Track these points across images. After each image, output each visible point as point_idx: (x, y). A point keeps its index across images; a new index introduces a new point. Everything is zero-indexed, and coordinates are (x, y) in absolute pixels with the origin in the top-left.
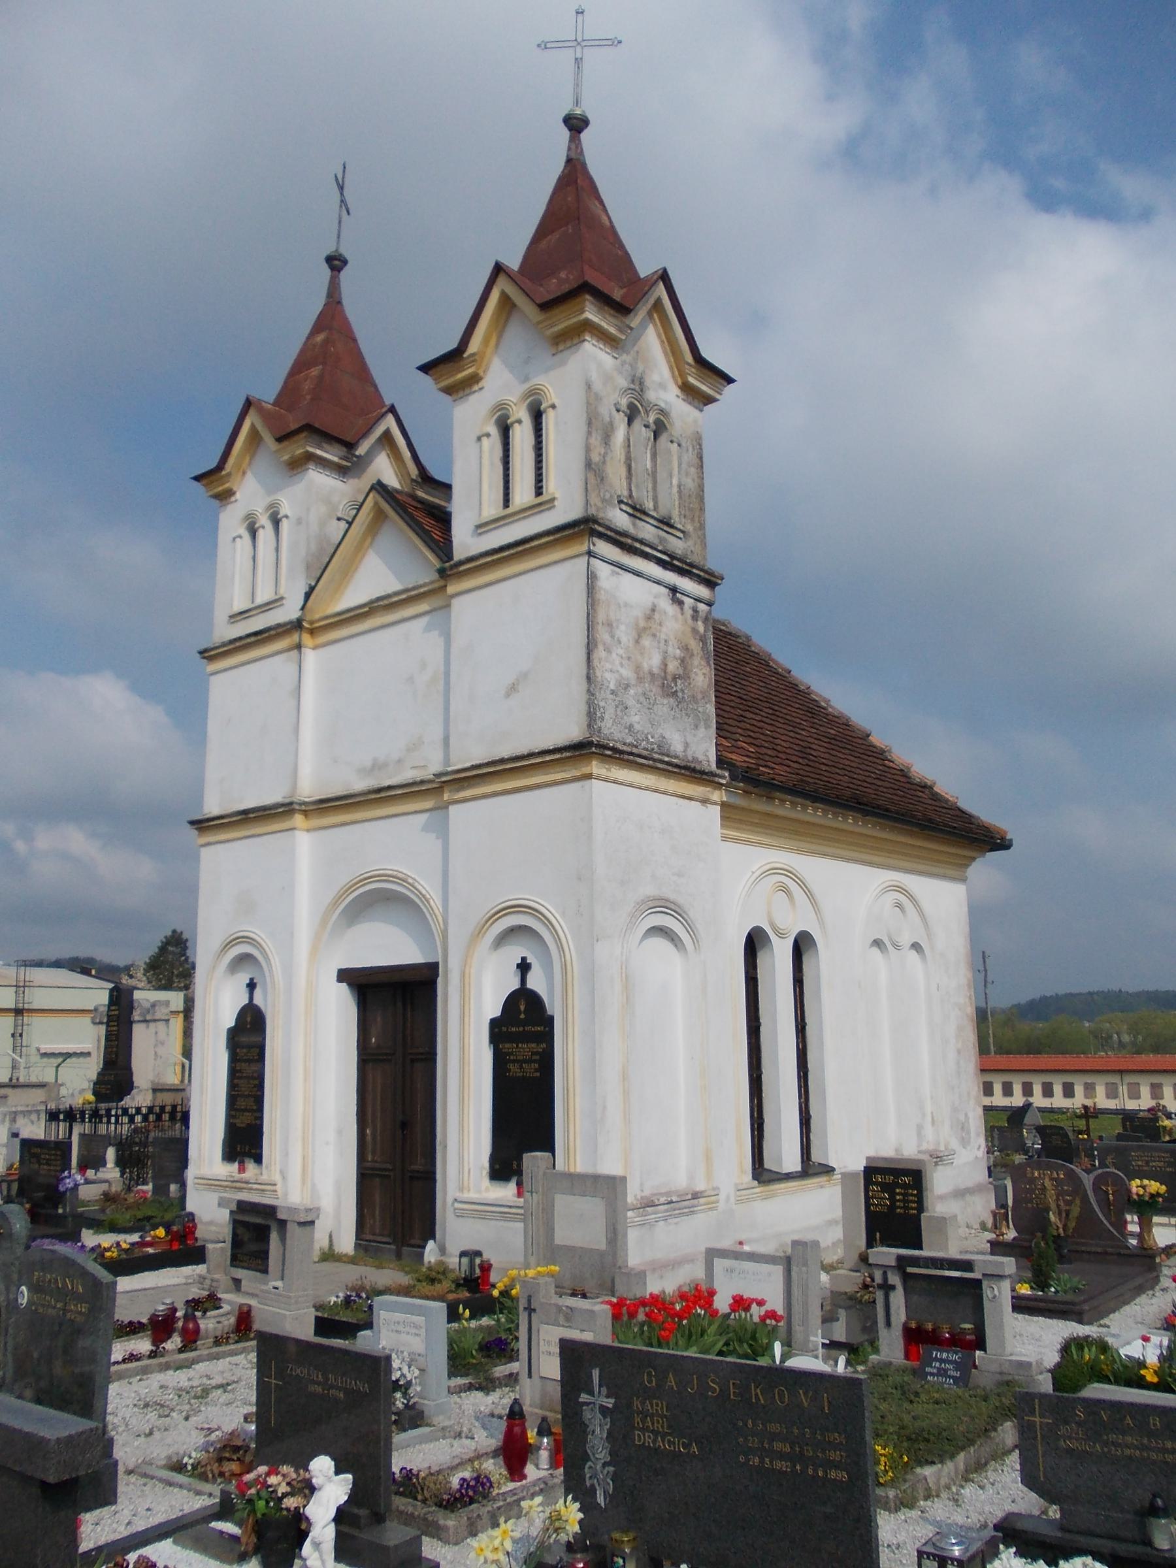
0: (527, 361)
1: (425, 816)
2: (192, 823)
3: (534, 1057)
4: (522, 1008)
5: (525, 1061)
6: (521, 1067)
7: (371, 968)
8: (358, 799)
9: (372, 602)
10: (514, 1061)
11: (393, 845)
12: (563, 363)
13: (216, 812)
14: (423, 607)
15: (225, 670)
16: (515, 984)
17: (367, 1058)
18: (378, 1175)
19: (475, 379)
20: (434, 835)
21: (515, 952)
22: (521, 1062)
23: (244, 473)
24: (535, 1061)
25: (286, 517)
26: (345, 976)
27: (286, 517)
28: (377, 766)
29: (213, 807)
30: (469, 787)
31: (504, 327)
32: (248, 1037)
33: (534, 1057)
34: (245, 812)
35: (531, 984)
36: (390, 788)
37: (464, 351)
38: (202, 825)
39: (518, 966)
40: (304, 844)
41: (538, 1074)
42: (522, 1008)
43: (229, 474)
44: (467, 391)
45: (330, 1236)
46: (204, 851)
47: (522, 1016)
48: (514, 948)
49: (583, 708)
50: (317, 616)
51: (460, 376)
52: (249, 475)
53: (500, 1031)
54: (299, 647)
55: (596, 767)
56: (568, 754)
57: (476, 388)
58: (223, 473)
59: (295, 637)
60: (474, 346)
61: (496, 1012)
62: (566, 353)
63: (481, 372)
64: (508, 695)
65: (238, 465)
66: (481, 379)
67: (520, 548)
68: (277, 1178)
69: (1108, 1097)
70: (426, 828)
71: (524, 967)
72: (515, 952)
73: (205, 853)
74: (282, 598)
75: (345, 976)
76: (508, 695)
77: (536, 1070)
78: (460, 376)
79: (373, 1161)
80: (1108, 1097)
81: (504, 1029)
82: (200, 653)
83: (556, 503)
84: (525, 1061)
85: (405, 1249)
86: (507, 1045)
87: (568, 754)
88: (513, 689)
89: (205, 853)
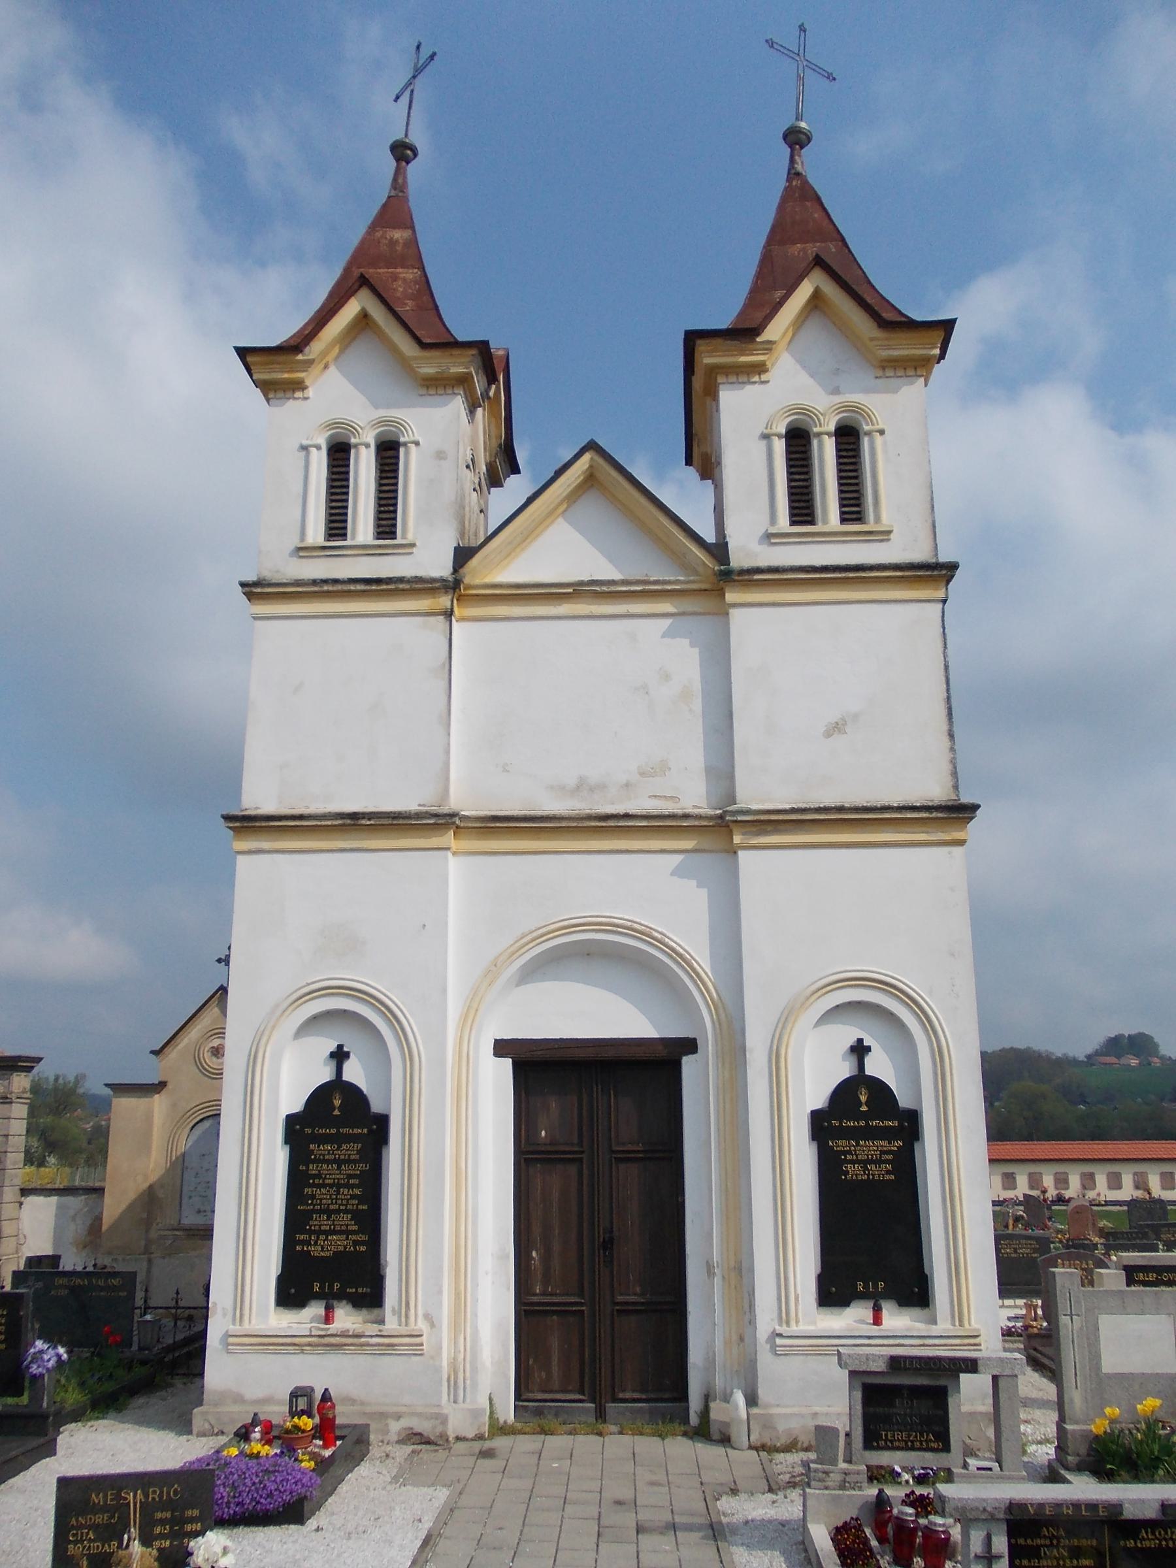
0: (837, 372)
1: (679, 858)
2: (228, 818)
3: (885, 1157)
4: (863, 1098)
5: (871, 1162)
6: (339, 1168)
7: (561, 1040)
8: (564, 824)
9: (581, 583)
10: (853, 1162)
11: (654, 893)
12: (895, 391)
13: (268, 807)
14: (667, 607)
15: (774, 604)
16: (326, 1074)
17: (529, 1157)
18: (554, 1312)
19: (299, 386)
20: (694, 883)
21: (847, 1033)
22: (864, 1163)
23: (326, 367)
24: (887, 1162)
25: (417, 444)
26: (502, 1048)
27: (417, 444)
28: (581, 787)
29: (259, 797)
30: (776, 831)
31: (350, 343)
32: (340, 1138)
33: (885, 1157)
34: (354, 816)
35: (870, 1070)
36: (627, 816)
37: (758, 335)
38: (246, 824)
39: (332, 1055)
40: (458, 875)
41: (893, 1177)
42: (863, 1098)
43: (311, 362)
44: (289, 394)
45: (491, 1399)
46: (241, 859)
47: (336, 1112)
48: (847, 1028)
49: (946, 767)
50: (477, 581)
51: (743, 359)
52: (332, 369)
53: (299, 1131)
54: (449, 614)
55: (448, 838)
56: (940, 815)
57: (298, 394)
58: (300, 357)
59: (444, 601)
60: (315, 348)
61: (297, 1106)
62: (900, 381)
63: (769, 364)
64: (828, 734)
65: (324, 353)
66: (766, 371)
67: (851, 575)
68: (422, 1325)
69: (1110, 1188)
70: (677, 872)
71: (339, 1056)
72: (847, 1033)
73: (243, 863)
74: (413, 545)
75: (502, 1048)
76: (828, 734)
77: (888, 1172)
78: (743, 359)
79: (544, 1294)
80: (1110, 1188)
81: (835, 1123)
82: (243, 585)
83: (892, 536)
84: (871, 1162)
85: (610, 1406)
86: (840, 1142)
87: (940, 815)
88: (836, 728)
89: (243, 863)
